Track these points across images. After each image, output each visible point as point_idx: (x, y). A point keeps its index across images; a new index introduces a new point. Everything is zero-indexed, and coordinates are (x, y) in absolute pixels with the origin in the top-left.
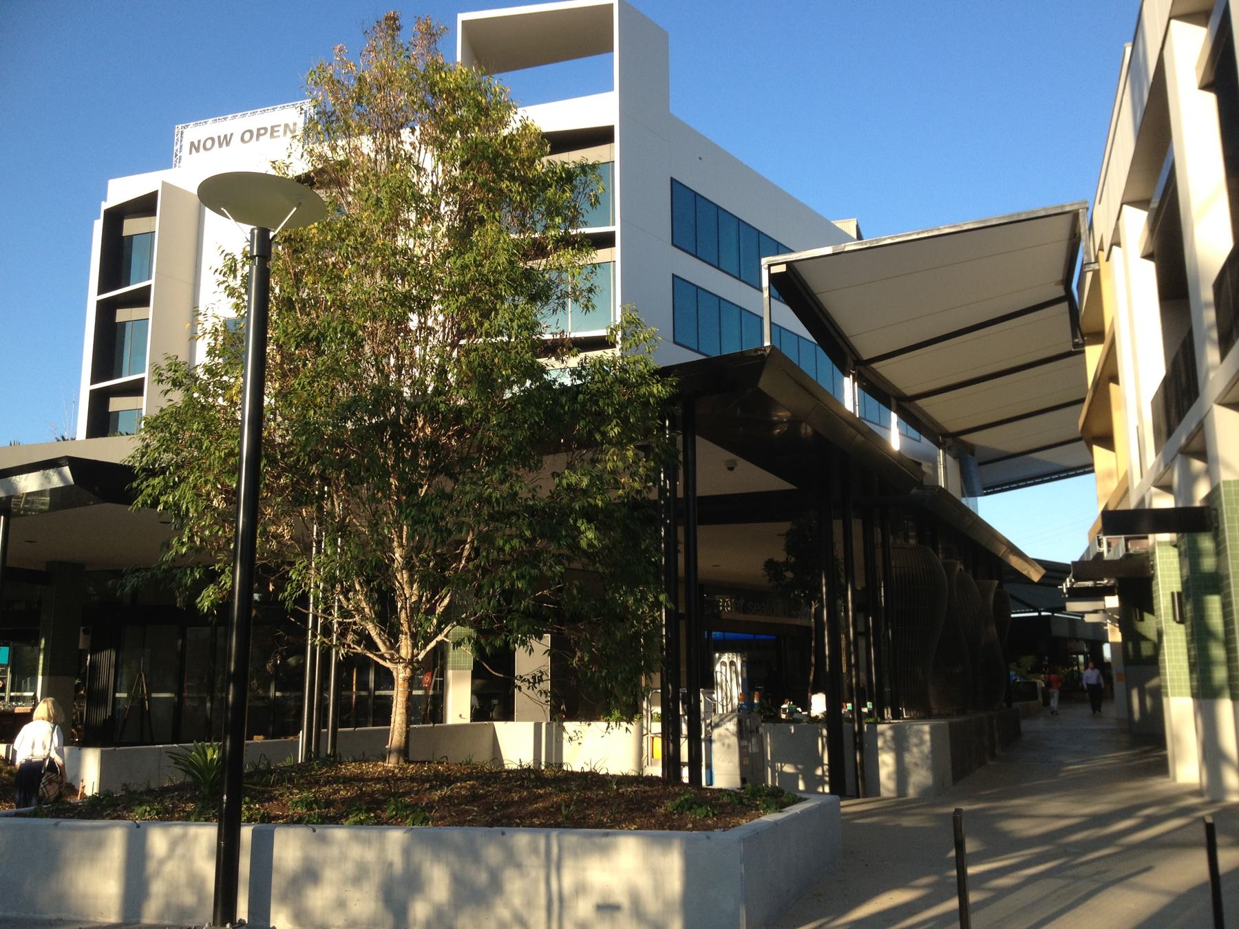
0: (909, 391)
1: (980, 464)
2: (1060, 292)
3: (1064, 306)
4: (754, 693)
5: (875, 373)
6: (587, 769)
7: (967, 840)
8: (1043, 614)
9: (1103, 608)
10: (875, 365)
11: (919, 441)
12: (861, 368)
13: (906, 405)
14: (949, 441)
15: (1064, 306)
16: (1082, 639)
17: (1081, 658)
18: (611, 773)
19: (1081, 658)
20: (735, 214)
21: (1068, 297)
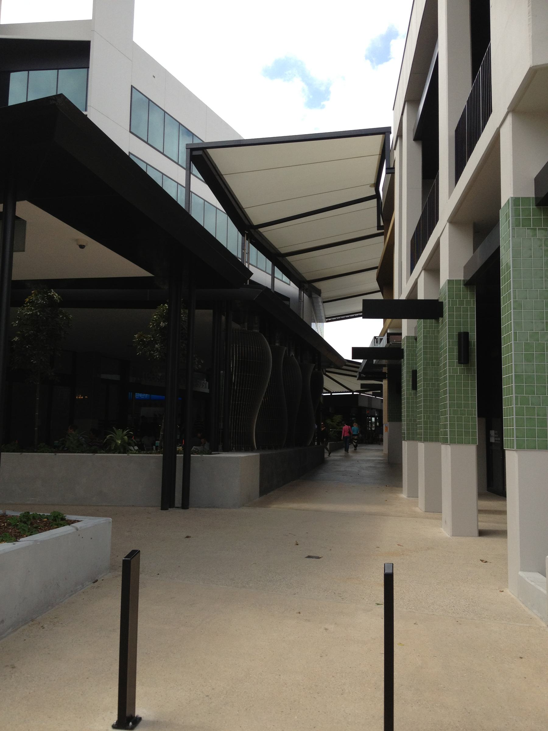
0: (283, 251)
1: (324, 302)
2: (373, 193)
3: (375, 201)
4: (162, 454)
5: (261, 234)
6: (512, 165)
7: (387, 361)
8: (355, 393)
9: (379, 408)
10: (261, 230)
11: (289, 285)
12: (252, 231)
13: (280, 259)
14: (306, 286)
15: (375, 201)
16: (375, 409)
17: (373, 419)
18: (512, 163)
19: (373, 419)
20: (64, 70)
21: (377, 196)
